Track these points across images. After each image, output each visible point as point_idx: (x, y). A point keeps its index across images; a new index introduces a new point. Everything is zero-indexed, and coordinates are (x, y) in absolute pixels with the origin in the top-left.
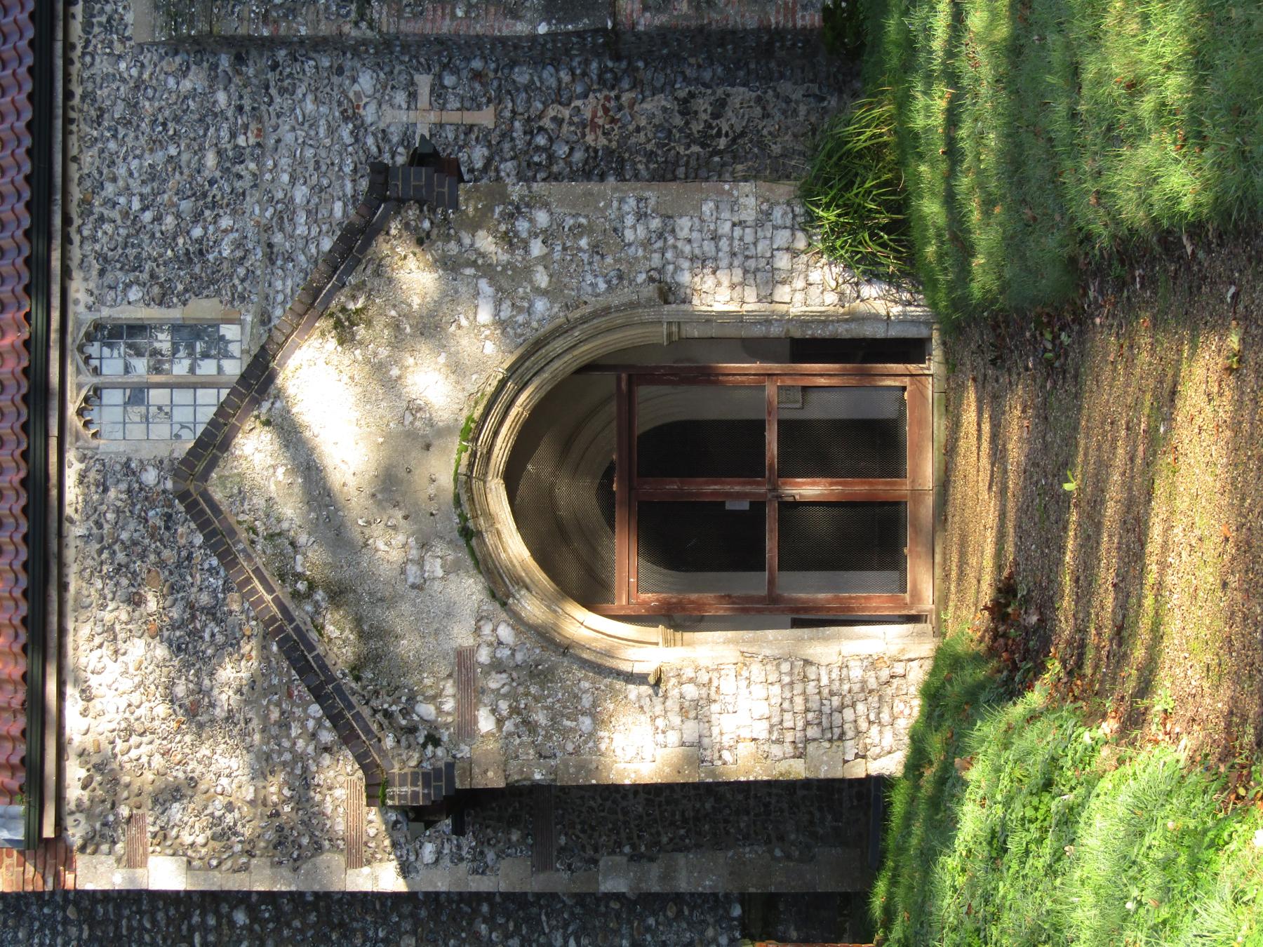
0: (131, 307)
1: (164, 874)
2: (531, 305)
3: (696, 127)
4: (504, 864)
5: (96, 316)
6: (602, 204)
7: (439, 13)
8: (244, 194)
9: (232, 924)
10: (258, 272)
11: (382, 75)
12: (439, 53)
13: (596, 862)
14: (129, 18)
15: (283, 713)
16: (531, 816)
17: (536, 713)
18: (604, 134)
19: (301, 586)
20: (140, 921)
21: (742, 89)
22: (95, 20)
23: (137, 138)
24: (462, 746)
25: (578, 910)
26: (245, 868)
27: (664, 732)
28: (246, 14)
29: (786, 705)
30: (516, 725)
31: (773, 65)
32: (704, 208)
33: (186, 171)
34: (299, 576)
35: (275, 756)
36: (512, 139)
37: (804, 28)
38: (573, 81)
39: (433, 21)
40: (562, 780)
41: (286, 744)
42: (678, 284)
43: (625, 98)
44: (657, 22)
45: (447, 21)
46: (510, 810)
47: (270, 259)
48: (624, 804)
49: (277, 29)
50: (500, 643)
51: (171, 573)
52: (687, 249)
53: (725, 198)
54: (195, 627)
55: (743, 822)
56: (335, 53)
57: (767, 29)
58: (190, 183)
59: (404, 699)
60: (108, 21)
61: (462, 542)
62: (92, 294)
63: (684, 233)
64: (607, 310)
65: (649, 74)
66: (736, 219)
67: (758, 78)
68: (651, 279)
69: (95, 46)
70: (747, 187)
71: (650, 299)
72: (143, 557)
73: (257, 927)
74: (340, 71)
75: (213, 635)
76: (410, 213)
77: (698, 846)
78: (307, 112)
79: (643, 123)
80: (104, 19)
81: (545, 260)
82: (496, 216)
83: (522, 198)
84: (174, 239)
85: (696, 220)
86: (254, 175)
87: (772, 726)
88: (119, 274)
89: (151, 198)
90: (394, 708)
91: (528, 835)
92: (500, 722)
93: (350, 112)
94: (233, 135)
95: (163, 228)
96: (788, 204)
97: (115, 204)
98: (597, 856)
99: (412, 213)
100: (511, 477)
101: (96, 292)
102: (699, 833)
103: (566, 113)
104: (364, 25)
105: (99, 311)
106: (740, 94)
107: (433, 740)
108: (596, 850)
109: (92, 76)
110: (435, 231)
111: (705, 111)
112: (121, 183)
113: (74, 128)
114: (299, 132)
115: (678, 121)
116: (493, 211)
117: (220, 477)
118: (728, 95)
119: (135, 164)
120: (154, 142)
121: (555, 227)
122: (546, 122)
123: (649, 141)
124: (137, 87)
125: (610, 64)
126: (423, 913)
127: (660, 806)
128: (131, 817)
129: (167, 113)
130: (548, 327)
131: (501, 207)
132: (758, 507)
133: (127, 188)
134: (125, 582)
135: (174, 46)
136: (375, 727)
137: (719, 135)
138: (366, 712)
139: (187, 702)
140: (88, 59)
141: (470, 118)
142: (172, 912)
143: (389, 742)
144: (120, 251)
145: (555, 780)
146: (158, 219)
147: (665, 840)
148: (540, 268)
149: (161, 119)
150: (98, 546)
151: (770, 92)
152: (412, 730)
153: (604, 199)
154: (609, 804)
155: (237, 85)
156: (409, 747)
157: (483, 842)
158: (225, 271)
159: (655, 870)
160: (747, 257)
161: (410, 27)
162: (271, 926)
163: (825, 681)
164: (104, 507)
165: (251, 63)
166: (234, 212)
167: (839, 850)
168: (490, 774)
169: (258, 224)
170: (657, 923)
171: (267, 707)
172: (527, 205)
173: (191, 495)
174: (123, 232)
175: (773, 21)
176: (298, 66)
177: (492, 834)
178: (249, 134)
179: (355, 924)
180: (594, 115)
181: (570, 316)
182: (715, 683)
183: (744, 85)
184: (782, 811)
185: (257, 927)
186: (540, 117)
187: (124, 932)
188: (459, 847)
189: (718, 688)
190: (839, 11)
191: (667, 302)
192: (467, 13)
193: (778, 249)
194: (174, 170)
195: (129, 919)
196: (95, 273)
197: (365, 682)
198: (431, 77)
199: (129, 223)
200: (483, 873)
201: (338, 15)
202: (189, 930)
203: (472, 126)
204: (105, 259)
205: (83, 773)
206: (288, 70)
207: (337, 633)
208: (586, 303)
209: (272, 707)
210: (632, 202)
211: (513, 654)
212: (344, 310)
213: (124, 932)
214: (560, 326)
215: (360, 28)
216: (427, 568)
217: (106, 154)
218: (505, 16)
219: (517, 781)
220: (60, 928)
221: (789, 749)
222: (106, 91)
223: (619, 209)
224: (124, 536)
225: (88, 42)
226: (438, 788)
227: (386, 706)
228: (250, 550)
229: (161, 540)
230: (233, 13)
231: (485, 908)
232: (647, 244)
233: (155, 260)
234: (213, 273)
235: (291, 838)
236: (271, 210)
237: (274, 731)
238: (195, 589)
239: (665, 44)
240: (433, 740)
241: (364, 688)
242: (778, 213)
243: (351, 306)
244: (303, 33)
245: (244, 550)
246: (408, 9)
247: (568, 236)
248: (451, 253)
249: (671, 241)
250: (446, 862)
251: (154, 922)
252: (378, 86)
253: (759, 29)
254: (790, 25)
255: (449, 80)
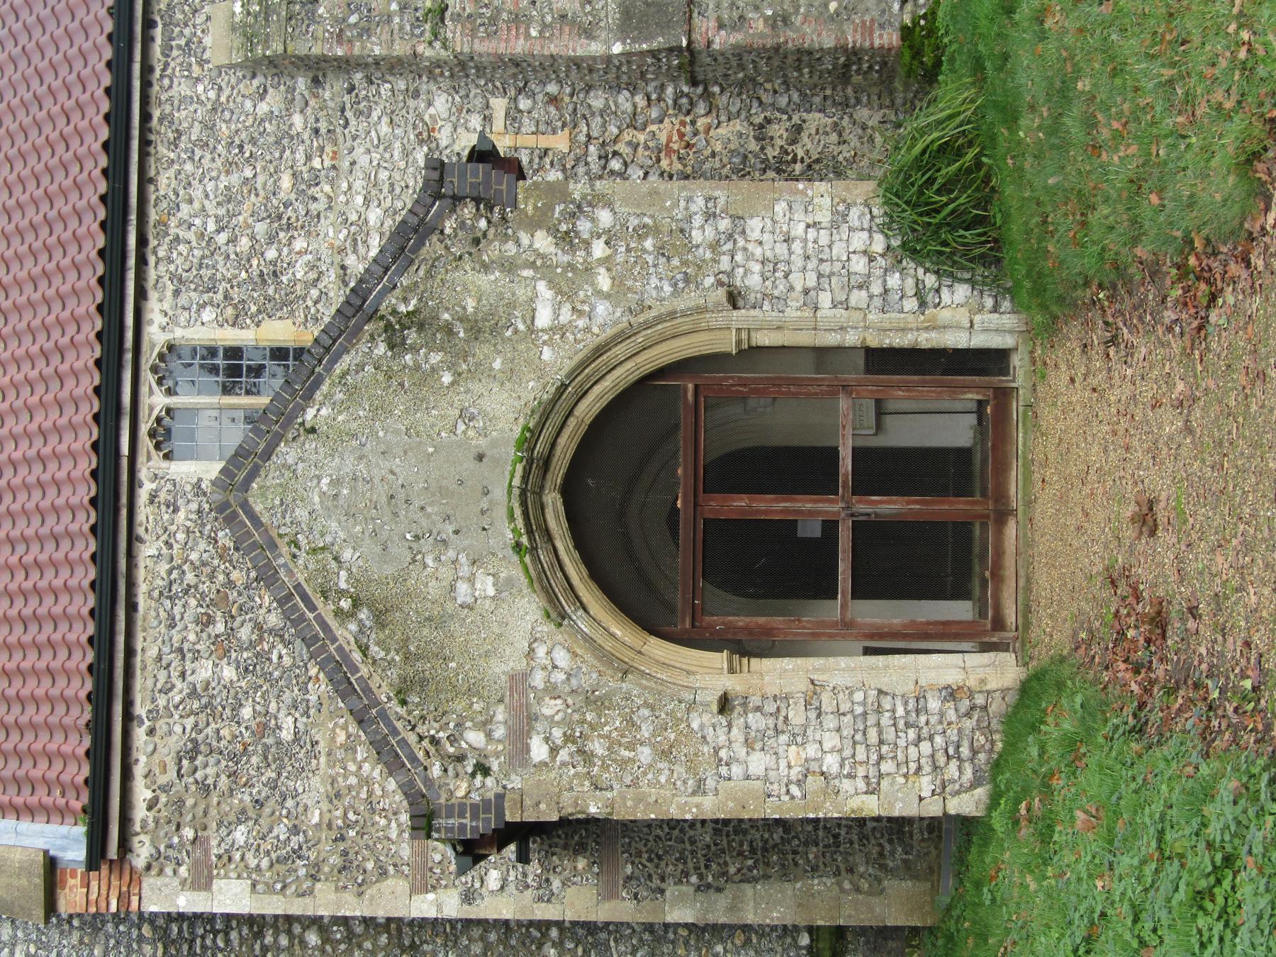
0: (204, 328)
1: (231, 896)
2: (593, 309)
3: (771, 153)
4: (571, 891)
5: (169, 336)
6: (668, 204)
7: (514, 32)
8: (318, 216)
9: (303, 943)
10: (331, 294)
11: (457, 98)
12: (514, 76)
13: (662, 891)
14: (208, 41)
15: (349, 736)
16: (597, 844)
17: (593, 741)
18: (679, 158)
19: (345, 604)
20: (214, 941)
21: (818, 115)
22: (173, 43)
23: (213, 160)
24: (513, 777)
25: (647, 936)
26: (310, 892)
27: (727, 764)
28: (320, 34)
29: (859, 737)
30: (571, 755)
31: (849, 91)
32: (777, 208)
33: (262, 193)
34: (342, 593)
35: (340, 779)
36: (587, 164)
37: (882, 47)
38: (649, 105)
39: (507, 41)
40: (619, 813)
41: (352, 767)
42: (748, 288)
43: (701, 123)
44: (732, 40)
45: (521, 41)
46: (576, 838)
47: (344, 281)
48: (691, 833)
49: (351, 49)
50: (555, 667)
51: (240, 594)
52: (758, 252)
53: (799, 198)
54: (263, 649)
55: (813, 852)
56: (411, 76)
57: (844, 49)
58: (265, 206)
59: (452, 725)
60: (187, 44)
61: (515, 558)
62: (166, 315)
63: (756, 235)
64: (672, 315)
65: (725, 98)
66: (810, 221)
67: (834, 104)
68: (720, 283)
69: (174, 69)
70: (822, 187)
71: (718, 304)
72: (212, 577)
73: (328, 948)
74: (416, 94)
75: (280, 657)
76: (466, 211)
77: (766, 877)
78: (382, 134)
79: (718, 148)
80: (183, 42)
81: (606, 262)
82: (556, 215)
83: (584, 197)
84: (249, 260)
85: (768, 221)
86: (329, 197)
87: (843, 760)
88: (194, 295)
89: (226, 219)
90: (441, 734)
91: (594, 863)
92: (554, 751)
93: (425, 135)
94: (309, 158)
95: (238, 249)
96: (866, 204)
97: (190, 226)
98: (663, 886)
99: (468, 211)
100: (568, 491)
101: (170, 313)
102: (767, 864)
103: (642, 137)
104: (437, 44)
105: (172, 331)
106: (815, 120)
107: (483, 769)
108: (663, 879)
109: (170, 99)
110: (492, 231)
111: (781, 137)
112: (197, 205)
113: (152, 150)
114: (374, 155)
115: (753, 146)
116: (554, 210)
117: (260, 488)
118: (804, 121)
119: (210, 186)
120: (231, 164)
121: (618, 227)
122: (621, 147)
123: (724, 166)
124: (214, 109)
125: (686, 89)
126: (493, 937)
127: (728, 836)
128: (195, 839)
129: (244, 135)
130: (610, 332)
131: (562, 207)
132: (830, 527)
133: (203, 209)
134: (193, 602)
135: (253, 67)
136: (421, 755)
137: (794, 161)
138: (412, 738)
139: (253, 724)
140: (166, 82)
141: (544, 142)
142: (245, 931)
143: (436, 771)
144: (195, 273)
145: (611, 814)
146: (232, 241)
147: (732, 870)
148: (602, 270)
149: (237, 142)
150: (168, 567)
151: (846, 118)
152: (460, 758)
153: (670, 198)
154: (676, 832)
155: (314, 108)
156: (457, 775)
157: (549, 869)
158: (299, 293)
159: (722, 901)
160: (822, 260)
161: (483, 47)
162: (343, 947)
163: (900, 711)
164: (174, 528)
165: (328, 86)
166: (309, 233)
167: (909, 883)
168: (543, 806)
169: (332, 246)
170: (726, 951)
171: (333, 730)
172: (590, 204)
173: (230, 506)
174: (197, 253)
175: (850, 40)
176: (373, 89)
177: (558, 862)
178: (324, 157)
179: (425, 946)
180: (669, 140)
181: (633, 320)
182: (783, 713)
183: (820, 111)
184: (851, 843)
185: (328, 948)
186: (615, 141)
187: (198, 951)
188: (525, 875)
189: (786, 718)
190: (918, 29)
191: (735, 307)
192: (540, 32)
193: (854, 252)
194: (250, 192)
195: (203, 937)
196: (169, 294)
197: (410, 707)
198: (506, 100)
199: (204, 244)
200: (549, 901)
201: (413, 35)
202: (261, 949)
203: (546, 151)
204: (180, 280)
205: (149, 795)
206: (364, 92)
207: (382, 654)
208: (650, 308)
209: (338, 731)
210: (700, 202)
211: (568, 679)
212: (394, 312)
213: (198, 951)
214: (623, 331)
215: (434, 48)
216: (478, 586)
217: (182, 176)
218: (580, 36)
219: (571, 814)
220: (135, 946)
221: (861, 785)
222: (184, 113)
223: (687, 209)
224: (194, 556)
225: (166, 65)
226: (488, 821)
227: (433, 732)
228: (291, 565)
229: (231, 561)
230: (307, 32)
231: (554, 933)
232: (715, 246)
233: (230, 281)
234: (287, 295)
235: (356, 863)
236: (345, 232)
237: (340, 754)
238: (263, 611)
239: (742, 67)
240: (483, 769)
241: (409, 713)
242: (854, 213)
243: (402, 309)
244: (377, 53)
245: (285, 565)
246: (482, 29)
247: (632, 237)
248: (509, 254)
249: (741, 243)
250: (511, 888)
251: (228, 941)
252: (454, 109)
253: (836, 49)
254: (867, 44)
255: (524, 104)
